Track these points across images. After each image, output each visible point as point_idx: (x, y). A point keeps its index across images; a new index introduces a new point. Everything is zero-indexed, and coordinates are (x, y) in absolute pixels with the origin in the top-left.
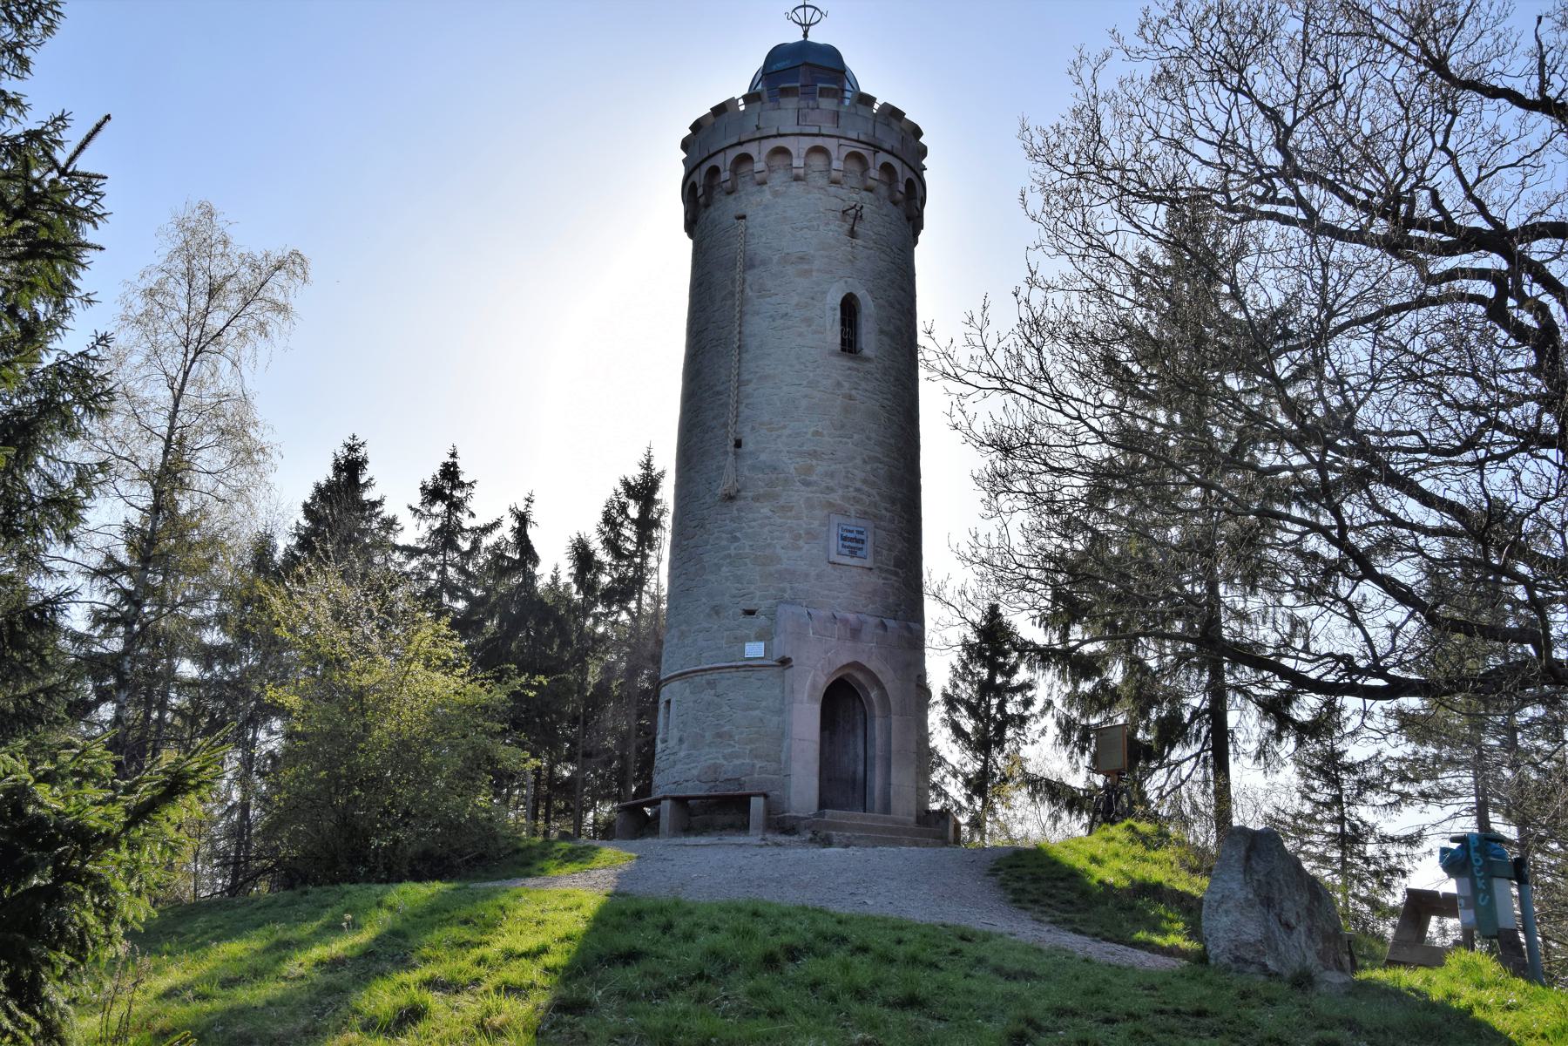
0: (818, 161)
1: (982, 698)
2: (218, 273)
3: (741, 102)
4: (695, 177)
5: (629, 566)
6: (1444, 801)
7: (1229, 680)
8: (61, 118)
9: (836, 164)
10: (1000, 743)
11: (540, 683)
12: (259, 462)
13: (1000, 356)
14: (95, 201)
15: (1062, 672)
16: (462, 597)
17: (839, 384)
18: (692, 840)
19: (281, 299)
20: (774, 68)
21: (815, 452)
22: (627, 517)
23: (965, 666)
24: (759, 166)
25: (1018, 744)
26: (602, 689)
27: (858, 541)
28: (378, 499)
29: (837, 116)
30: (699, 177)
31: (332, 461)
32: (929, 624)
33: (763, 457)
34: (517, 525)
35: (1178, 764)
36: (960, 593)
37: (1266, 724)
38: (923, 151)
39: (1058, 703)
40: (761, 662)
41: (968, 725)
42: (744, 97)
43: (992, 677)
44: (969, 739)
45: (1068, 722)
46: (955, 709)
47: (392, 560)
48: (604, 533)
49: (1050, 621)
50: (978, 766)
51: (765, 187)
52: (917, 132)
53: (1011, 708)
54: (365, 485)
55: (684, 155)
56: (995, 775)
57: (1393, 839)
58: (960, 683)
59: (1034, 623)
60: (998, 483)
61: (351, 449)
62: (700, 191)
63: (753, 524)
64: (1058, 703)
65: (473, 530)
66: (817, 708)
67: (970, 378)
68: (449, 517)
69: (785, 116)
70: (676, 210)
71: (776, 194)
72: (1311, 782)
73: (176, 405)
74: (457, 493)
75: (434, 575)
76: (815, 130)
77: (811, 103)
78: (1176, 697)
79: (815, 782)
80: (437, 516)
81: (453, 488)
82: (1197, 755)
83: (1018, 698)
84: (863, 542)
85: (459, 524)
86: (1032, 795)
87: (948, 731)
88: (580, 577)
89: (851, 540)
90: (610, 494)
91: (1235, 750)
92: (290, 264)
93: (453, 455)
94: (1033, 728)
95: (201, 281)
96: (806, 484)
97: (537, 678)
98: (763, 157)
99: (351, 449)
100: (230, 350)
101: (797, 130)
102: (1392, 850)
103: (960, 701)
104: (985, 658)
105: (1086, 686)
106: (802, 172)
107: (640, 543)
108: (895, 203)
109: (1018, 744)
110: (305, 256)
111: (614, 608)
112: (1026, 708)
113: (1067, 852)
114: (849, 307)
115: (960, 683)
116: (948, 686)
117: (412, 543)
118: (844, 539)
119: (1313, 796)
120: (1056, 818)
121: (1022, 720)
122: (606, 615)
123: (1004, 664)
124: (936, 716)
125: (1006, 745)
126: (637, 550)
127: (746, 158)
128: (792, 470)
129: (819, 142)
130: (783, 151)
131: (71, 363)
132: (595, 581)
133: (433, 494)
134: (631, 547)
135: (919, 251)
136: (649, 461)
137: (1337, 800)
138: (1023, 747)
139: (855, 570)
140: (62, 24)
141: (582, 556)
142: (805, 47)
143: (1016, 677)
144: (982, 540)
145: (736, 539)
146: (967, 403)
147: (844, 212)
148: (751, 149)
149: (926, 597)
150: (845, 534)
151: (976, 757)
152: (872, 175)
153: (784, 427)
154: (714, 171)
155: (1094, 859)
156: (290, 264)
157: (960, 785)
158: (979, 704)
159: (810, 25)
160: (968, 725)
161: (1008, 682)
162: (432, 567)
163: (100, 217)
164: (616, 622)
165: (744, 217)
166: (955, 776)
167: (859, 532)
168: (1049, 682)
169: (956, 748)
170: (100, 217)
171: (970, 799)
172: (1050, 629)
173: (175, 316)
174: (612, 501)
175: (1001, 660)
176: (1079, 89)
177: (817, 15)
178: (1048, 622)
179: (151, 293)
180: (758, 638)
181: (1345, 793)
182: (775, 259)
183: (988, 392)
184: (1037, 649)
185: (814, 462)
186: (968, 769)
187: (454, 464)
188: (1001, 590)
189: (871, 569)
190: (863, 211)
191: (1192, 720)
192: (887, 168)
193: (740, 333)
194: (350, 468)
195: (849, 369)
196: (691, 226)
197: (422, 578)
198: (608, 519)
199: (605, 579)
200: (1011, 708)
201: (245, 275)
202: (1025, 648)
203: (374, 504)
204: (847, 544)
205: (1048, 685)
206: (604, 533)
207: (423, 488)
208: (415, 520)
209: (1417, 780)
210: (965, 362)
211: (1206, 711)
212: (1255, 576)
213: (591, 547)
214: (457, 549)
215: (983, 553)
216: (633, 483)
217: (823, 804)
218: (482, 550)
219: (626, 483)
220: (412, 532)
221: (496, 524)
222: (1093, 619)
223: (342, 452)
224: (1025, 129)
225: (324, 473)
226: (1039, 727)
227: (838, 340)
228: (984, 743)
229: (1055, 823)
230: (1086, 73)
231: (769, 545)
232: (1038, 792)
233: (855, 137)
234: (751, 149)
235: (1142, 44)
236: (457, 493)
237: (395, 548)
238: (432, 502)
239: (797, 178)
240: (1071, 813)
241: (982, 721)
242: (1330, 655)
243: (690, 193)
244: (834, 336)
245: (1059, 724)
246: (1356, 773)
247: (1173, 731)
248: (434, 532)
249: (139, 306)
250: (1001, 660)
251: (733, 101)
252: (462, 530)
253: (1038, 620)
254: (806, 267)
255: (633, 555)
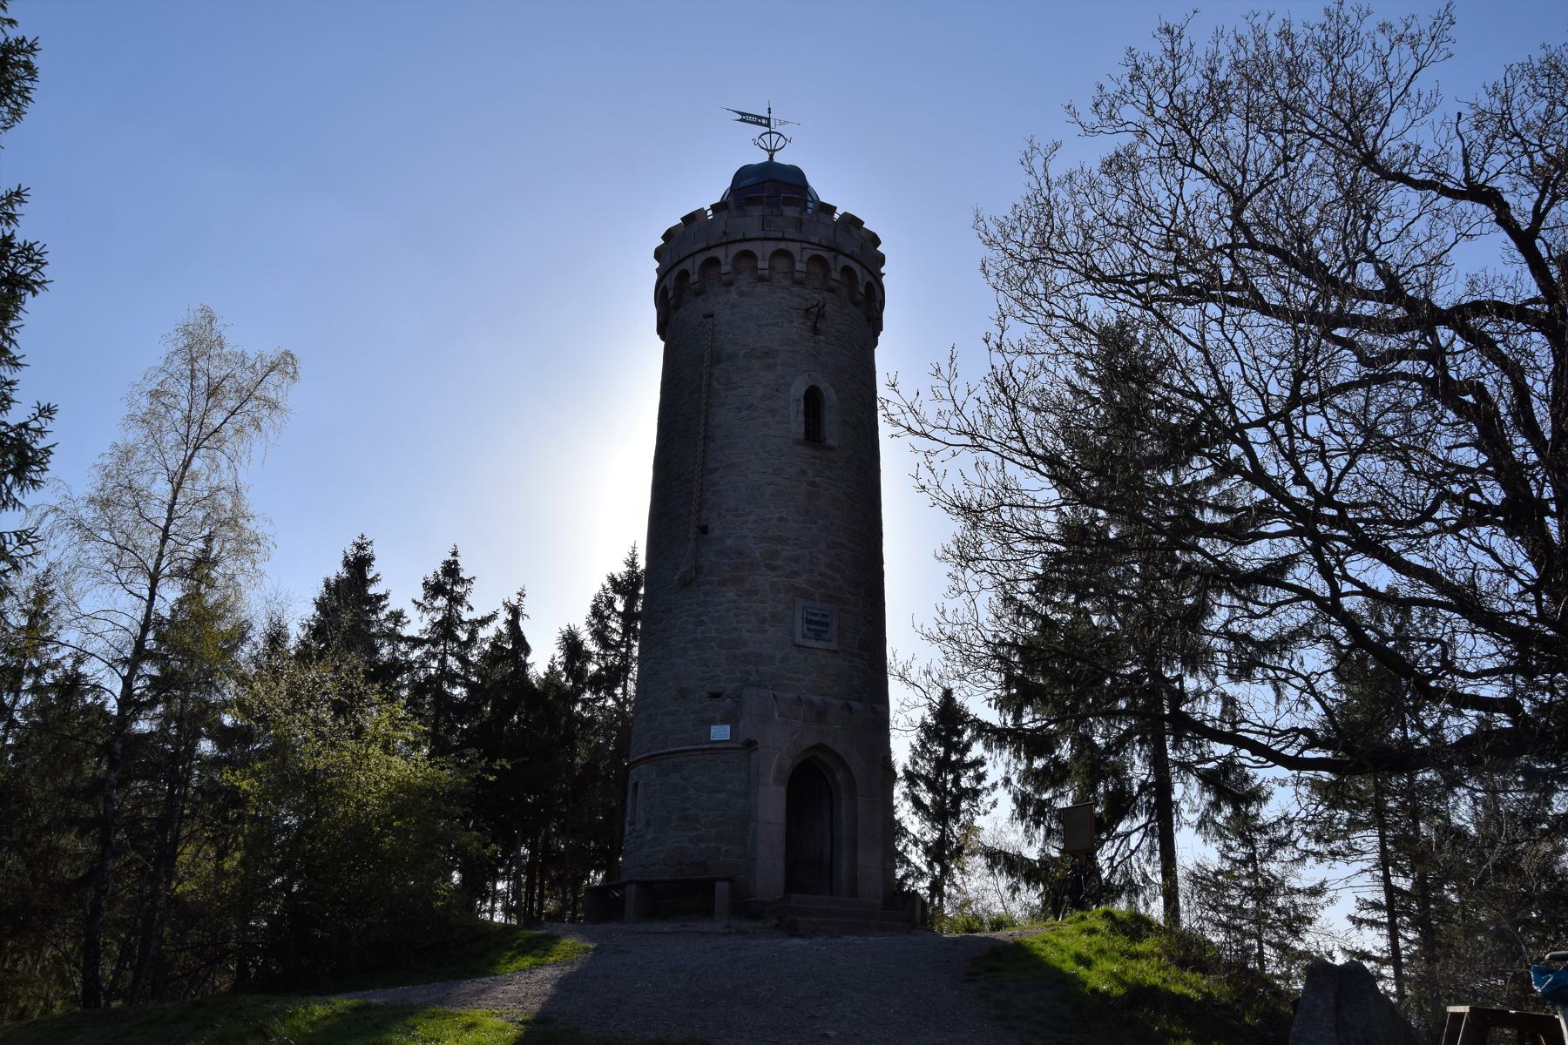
0: (782, 265)
1: (938, 774)
2: (216, 374)
3: (710, 213)
4: (667, 281)
5: (616, 656)
6: (1350, 858)
7: (1171, 754)
8: (18, 194)
9: (798, 266)
10: (956, 813)
11: (503, 767)
12: (252, 552)
13: (971, 409)
14: (35, 269)
15: (1018, 750)
16: (460, 684)
17: (803, 472)
18: (655, 926)
19: (273, 396)
20: (742, 184)
21: (780, 536)
22: (614, 610)
23: (923, 745)
24: (726, 268)
25: (972, 814)
26: (591, 769)
27: (822, 624)
28: (383, 593)
29: (799, 223)
30: (670, 282)
31: (342, 558)
32: (894, 705)
33: (729, 542)
34: (510, 618)
35: (1127, 835)
36: (925, 674)
37: (1206, 795)
38: (881, 260)
39: (1014, 779)
40: (726, 745)
41: (927, 798)
42: (713, 207)
43: (947, 754)
44: (929, 811)
45: (1023, 798)
46: (917, 785)
47: (399, 650)
48: (592, 625)
49: (1004, 703)
50: (936, 835)
51: (732, 288)
52: (875, 240)
53: (965, 783)
54: (373, 581)
55: (657, 265)
56: (952, 843)
57: (1299, 891)
58: (919, 760)
59: (990, 705)
60: (966, 557)
61: (360, 547)
62: (670, 294)
63: (719, 608)
64: (1014, 779)
65: (471, 622)
66: (783, 790)
67: (937, 434)
68: (450, 611)
69: (751, 222)
70: (649, 315)
71: (742, 294)
72: (1228, 842)
73: (175, 498)
74: (458, 589)
75: (435, 664)
76: (780, 235)
77: (775, 211)
78: (1119, 771)
79: (781, 865)
80: (439, 609)
81: (455, 583)
82: (1145, 826)
83: (971, 773)
84: (827, 625)
85: (459, 617)
86: (991, 867)
87: (908, 805)
88: (569, 666)
89: (816, 623)
90: (597, 589)
91: (1178, 820)
92: (284, 364)
93: (455, 554)
94: (986, 801)
95: (202, 382)
96: (773, 568)
97: (498, 762)
98: (730, 259)
99: (360, 547)
100: (228, 446)
101: (761, 234)
102: (1299, 899)
103: (920, 776)
104: (941, 738)
105: (1039, 763)
106: (767, 272)
107: (624, 635)
108: (856, 304)
109: (972, 814)
110: (297, 356)
111: (602, 694)
112: (979, 783)
113: (1048, 949)
114: (813, 399)
115: (919, 760)
116: (908, 763)
117: (416, 634)
118: (809, 622)
119: (1231, 855)
120: (1015, 889)
121: (974, 794)
122: (594, 701)
123: (959, 743)
124: (899, 790)
125: (962, 816)
126: (622, 641)
127: (714, 262)
128: (758, 555)
129: (783, 245)
130: (749, 255)
131: (12, 434)
132: (583, 670)
133: (435, 589)
134: (617, 638)
135: (879, 353)
136: (633, 559)
137: (1251, 858)
138: (977, 817)
139: (819, 652)
140: (29, 108)
141: (571, 644)
142: (770, 166)
143: (969, 754)
144: (949, 616)
145: (702, 623)
146: (936, 460)
147: (807, 310)
148: (719, 253)
149: (890, 678)
150: (810, 617)
151: (934, 827)
152: (833, 277)
153: (750, 513)
154: (684, 274)
155: (1081, 960)
156: (284, 364)
157: (920, 852)
158: (936, 779)
159: (775, 150)
160: (927, 798)
161: (962, 759)
162: (434, 656)
163: (39, 284)
164: (604, 706)
165: (711, 316)
166: (916, 845)
167: (823, 615)
168: (1006, 760)
169: (916, 819)
170: (39, 284)
171: (930, 865)
172: (1005, 711)
173: (178, 415)
174: (600, 596)
175: (956, 739)
176: (1032, 178)
177: (782, 140)
178: (1002, 704)
179: (155, 395)
180: (724, 722)
181: (1258, 851)
182: (742, 353)
183: (957, 449)
184: (993, 729)
185: (779, 547)
186: (927, 838)
187: (455, 562)
188: (967, 669)
189: (835, 652)
190: (826, 308)
191: (1139, 793)
192: (847, 271)
193: (706, 424)
194: (359, 565)
195: (813, 457)
196: (662, 330)
197: (423, 665)
198: (596, 612)
199: (592, 668)
200: (965, 783)
201: (246, 378)
202: (982, 728)
203: (380, 598)
204: (811, 627)
205: (999, 765)
206: (592, 625)
207: (426, 584)
208: (419, 613)
209: (1328, 841)
210: (931, 417)
211: (1152, 784)
212: (1197, 659)
213: (581, 638)
214: (456, 639)
215: (948, 630)
216: (619, 580)
217: (792, 885)
218: (479, 641)
219: (612, 580)
220: (417, 624)
221: (492, 617)
222: (1045, 703)
223: (351, 551)
224: (979, 219)
225: (335, 569)
226: (991, 799)
227: (802, 430)
228: (941, 814)
229: (1014, 893)
230: (1038, 164)
231: (735, 628)
232: (997, 864)
233: (817, 241)
234: (719, 253)
235: (1095, 119)
236: (458, 589)
237: (401, 639)
238: (434, 597)
239: (762, 279)
240: (1028, 884)
241: (939, 795)
242: (1293, 729)
243: (663, 298)
244: (798, 426)
245: (1015, 799)
246: (1267, 833)
247: (1121, 805)
248: (435, 624)
249: (145, 403)
250: (956, 739)
251: (701, 211)
252: (462, 622)
253: (993, 702)
254: (771, 361)
255: (619, 645)
